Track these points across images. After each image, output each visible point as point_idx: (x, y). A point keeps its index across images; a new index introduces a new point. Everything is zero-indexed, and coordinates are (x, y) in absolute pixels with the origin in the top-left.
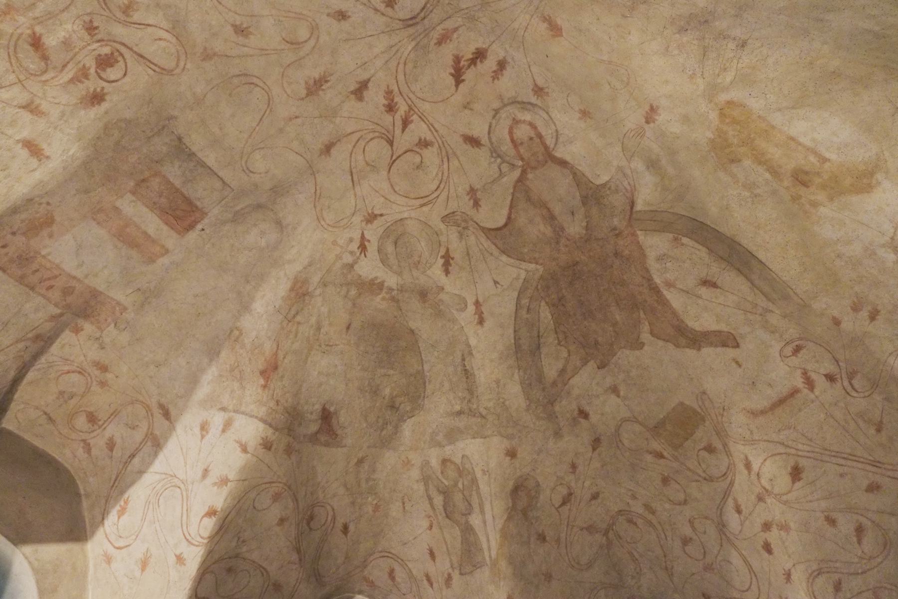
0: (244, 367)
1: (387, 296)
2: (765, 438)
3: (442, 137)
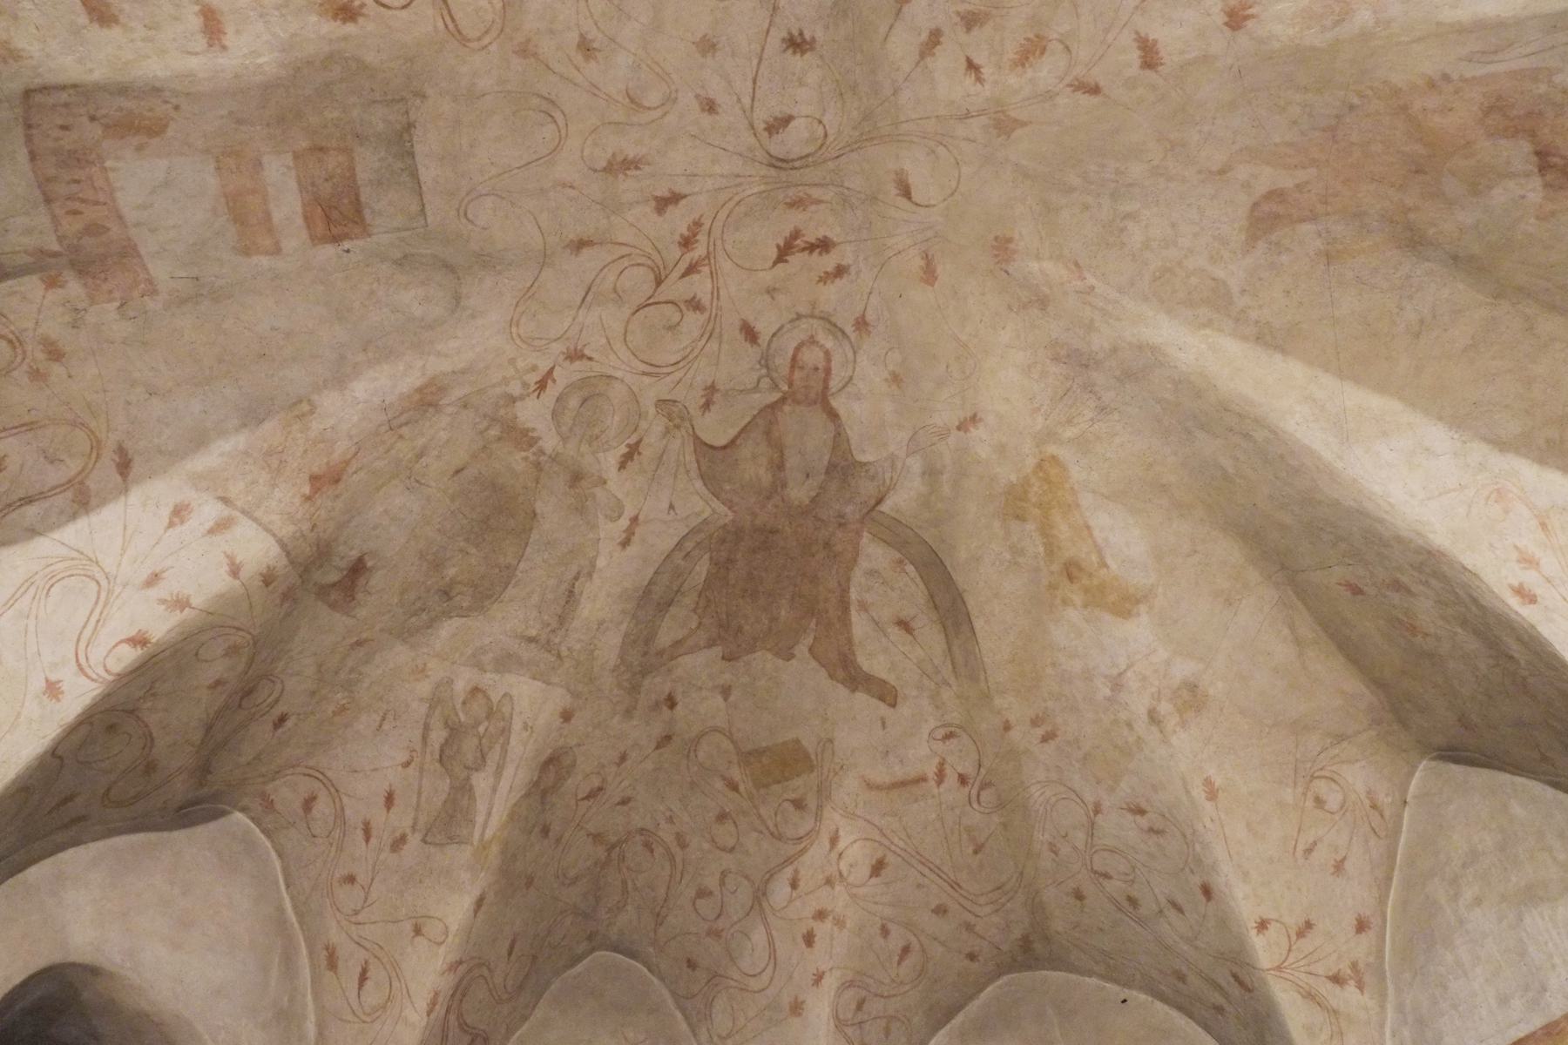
0: (291, 458)
1: (532, 458)
2: (868, 817)
3: (719, 308)
